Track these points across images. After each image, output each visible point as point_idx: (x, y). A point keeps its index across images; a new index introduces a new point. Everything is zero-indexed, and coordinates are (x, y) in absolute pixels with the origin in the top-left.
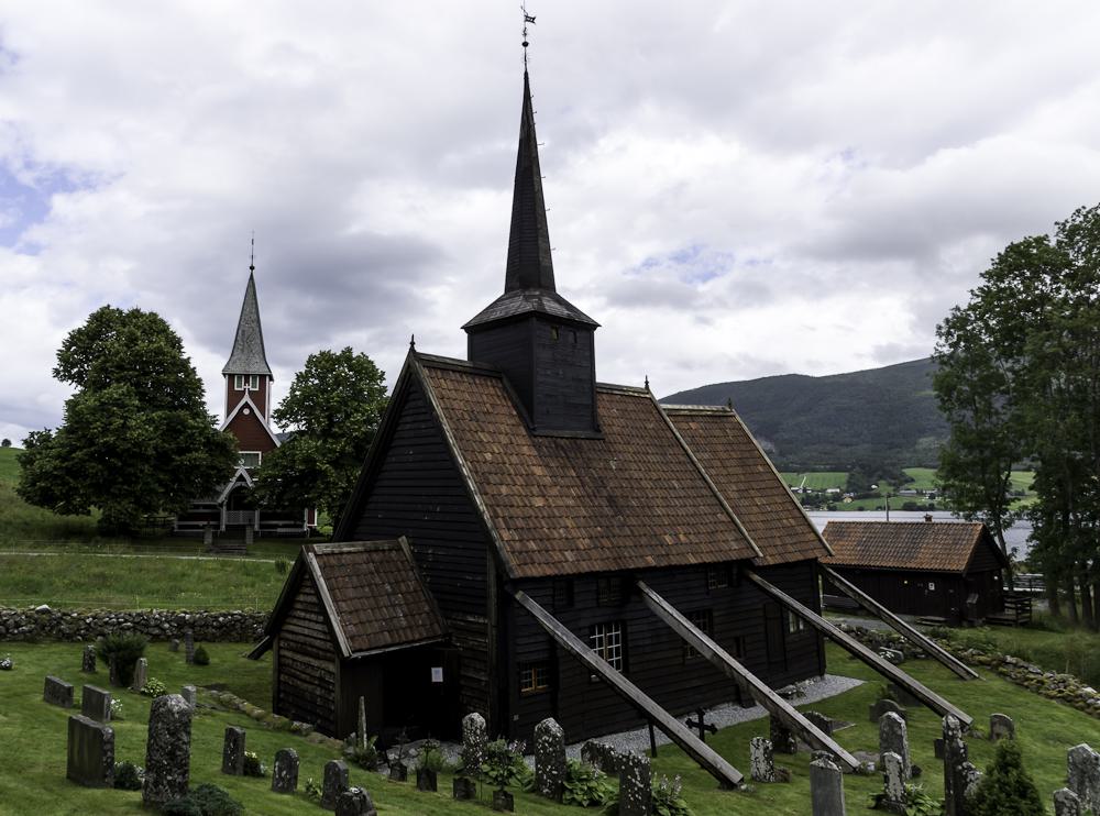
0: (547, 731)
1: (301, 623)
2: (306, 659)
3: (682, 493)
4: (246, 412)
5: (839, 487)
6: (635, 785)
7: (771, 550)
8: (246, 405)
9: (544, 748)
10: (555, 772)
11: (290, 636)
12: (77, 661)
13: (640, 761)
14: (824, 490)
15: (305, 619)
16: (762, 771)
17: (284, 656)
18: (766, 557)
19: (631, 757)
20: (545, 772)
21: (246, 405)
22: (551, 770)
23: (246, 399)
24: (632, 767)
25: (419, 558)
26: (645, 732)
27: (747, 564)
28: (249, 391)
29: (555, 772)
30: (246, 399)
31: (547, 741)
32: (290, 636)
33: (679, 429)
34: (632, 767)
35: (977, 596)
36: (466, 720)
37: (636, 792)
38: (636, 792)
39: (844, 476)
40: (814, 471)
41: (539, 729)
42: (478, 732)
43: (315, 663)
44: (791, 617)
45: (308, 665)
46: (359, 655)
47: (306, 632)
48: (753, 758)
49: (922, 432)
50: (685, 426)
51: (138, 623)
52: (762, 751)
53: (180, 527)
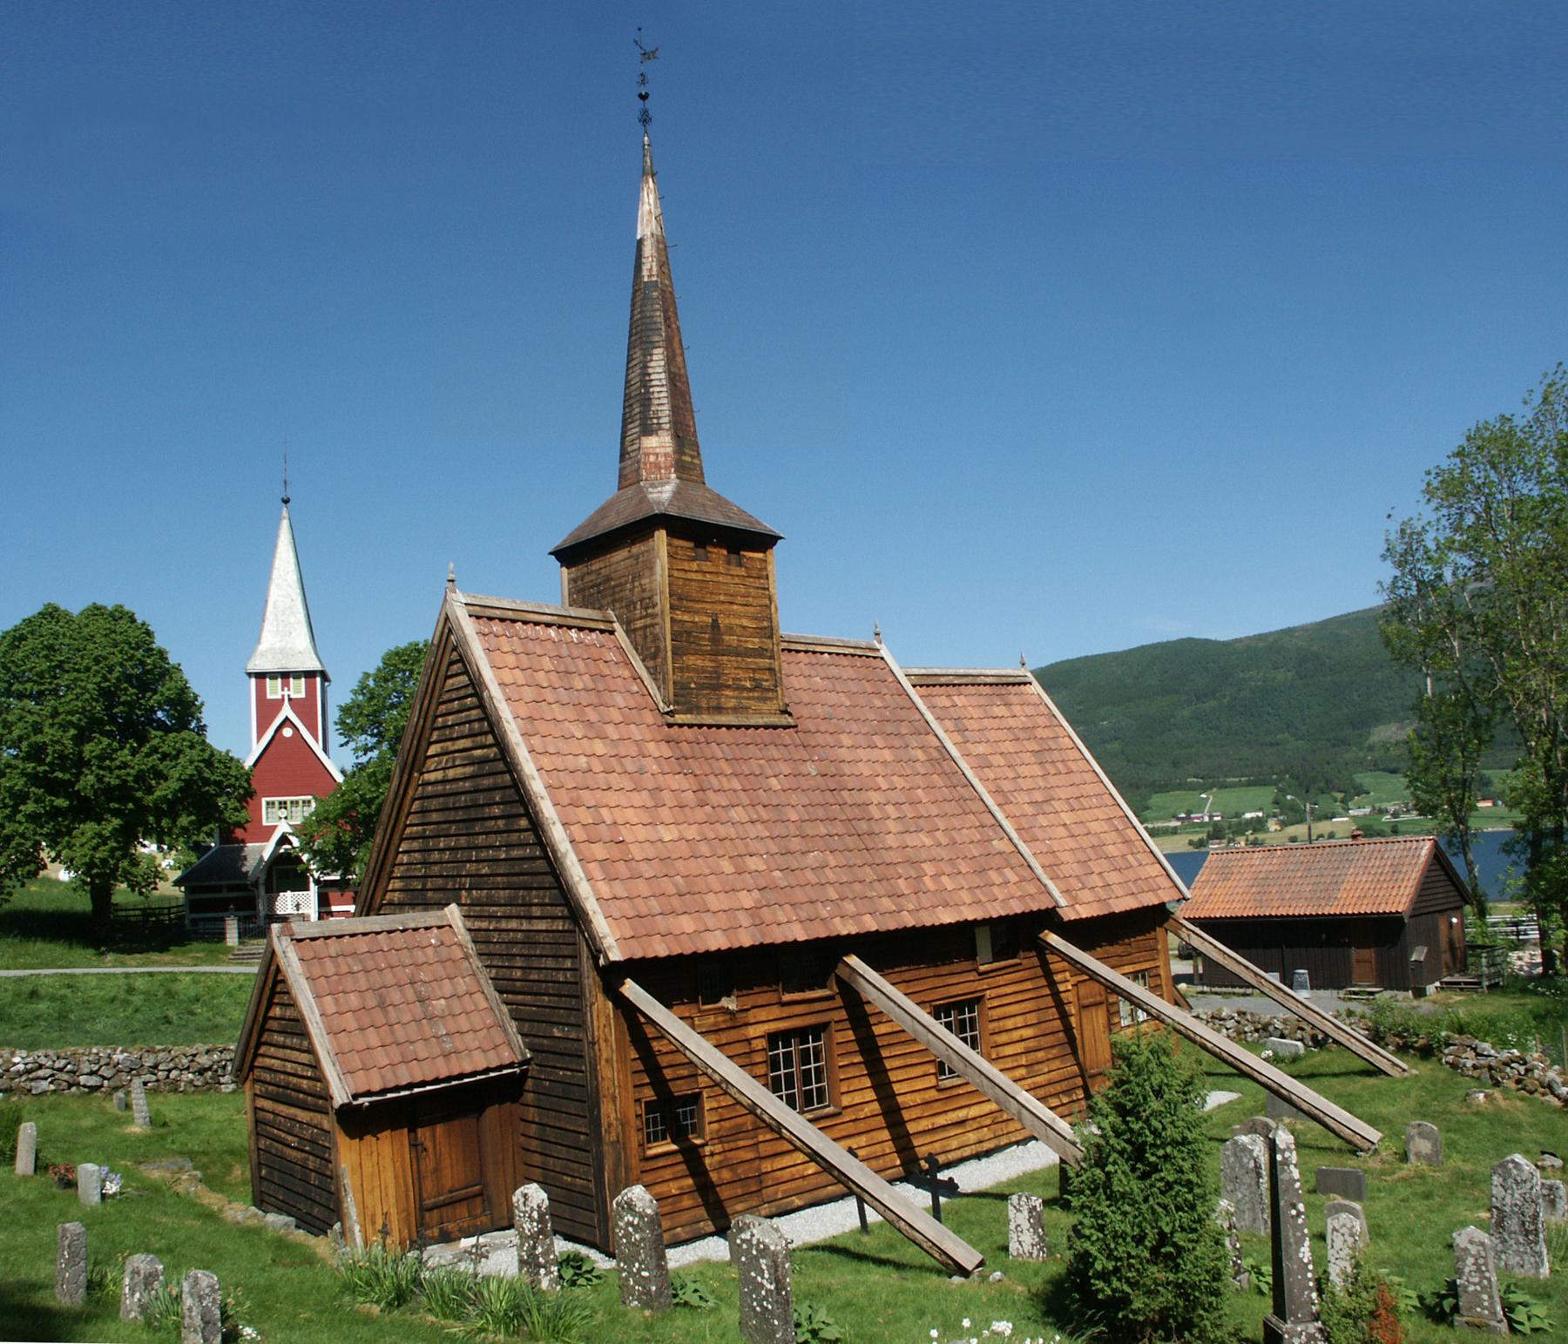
0: (630, 1207)
1: (281, 1053)
2: (292, 1111)
3: (934, 810)
4: (288, 732)
5: (1260, 809)
6: (763, 1286)
7: (1086, 895)
8: (287, 721)
9: (628, 1235)
10: (645, 1274)
11: (267, 1076)
12: (428, 1134)
13: (766, 1247)
14: (1238, 815)
15: (284, 1047)
16: (1027, 1247)
17: (262, 1109)
18: (1074, 910)
19: (754, 1242)
20: (630, 1273)
21: (287, 721)
22: (639, 1270)
23: (287, 711)
24: (756, 1258)
25: (478, 936)
26: (852, 1203)
27: (1049, 918)
28: (290, 699)
29: (645, 1274)
30: (287, 711)
31: (631, 1224)
32: (267, 1076)
33: (932, 707)
34: (756, 1258)
35: (1426, 950)
36: (517, 1197)
37: (765, 1298)
38: (765, 1298)
39: (1268, 794)
40: (1224, 786)
41: (618, 1204)
42: (535, 1215)
43: (303, 1115)
44: (1125, 1008)
45: (293, 1119)
46: (365, 1101)
47: (289, 1067)
48: (1012, 1226)
49: (1377, 718)
50: (943, 701)
51: (61, 1070)
52: (1026, 1213)
53: (194, 922)
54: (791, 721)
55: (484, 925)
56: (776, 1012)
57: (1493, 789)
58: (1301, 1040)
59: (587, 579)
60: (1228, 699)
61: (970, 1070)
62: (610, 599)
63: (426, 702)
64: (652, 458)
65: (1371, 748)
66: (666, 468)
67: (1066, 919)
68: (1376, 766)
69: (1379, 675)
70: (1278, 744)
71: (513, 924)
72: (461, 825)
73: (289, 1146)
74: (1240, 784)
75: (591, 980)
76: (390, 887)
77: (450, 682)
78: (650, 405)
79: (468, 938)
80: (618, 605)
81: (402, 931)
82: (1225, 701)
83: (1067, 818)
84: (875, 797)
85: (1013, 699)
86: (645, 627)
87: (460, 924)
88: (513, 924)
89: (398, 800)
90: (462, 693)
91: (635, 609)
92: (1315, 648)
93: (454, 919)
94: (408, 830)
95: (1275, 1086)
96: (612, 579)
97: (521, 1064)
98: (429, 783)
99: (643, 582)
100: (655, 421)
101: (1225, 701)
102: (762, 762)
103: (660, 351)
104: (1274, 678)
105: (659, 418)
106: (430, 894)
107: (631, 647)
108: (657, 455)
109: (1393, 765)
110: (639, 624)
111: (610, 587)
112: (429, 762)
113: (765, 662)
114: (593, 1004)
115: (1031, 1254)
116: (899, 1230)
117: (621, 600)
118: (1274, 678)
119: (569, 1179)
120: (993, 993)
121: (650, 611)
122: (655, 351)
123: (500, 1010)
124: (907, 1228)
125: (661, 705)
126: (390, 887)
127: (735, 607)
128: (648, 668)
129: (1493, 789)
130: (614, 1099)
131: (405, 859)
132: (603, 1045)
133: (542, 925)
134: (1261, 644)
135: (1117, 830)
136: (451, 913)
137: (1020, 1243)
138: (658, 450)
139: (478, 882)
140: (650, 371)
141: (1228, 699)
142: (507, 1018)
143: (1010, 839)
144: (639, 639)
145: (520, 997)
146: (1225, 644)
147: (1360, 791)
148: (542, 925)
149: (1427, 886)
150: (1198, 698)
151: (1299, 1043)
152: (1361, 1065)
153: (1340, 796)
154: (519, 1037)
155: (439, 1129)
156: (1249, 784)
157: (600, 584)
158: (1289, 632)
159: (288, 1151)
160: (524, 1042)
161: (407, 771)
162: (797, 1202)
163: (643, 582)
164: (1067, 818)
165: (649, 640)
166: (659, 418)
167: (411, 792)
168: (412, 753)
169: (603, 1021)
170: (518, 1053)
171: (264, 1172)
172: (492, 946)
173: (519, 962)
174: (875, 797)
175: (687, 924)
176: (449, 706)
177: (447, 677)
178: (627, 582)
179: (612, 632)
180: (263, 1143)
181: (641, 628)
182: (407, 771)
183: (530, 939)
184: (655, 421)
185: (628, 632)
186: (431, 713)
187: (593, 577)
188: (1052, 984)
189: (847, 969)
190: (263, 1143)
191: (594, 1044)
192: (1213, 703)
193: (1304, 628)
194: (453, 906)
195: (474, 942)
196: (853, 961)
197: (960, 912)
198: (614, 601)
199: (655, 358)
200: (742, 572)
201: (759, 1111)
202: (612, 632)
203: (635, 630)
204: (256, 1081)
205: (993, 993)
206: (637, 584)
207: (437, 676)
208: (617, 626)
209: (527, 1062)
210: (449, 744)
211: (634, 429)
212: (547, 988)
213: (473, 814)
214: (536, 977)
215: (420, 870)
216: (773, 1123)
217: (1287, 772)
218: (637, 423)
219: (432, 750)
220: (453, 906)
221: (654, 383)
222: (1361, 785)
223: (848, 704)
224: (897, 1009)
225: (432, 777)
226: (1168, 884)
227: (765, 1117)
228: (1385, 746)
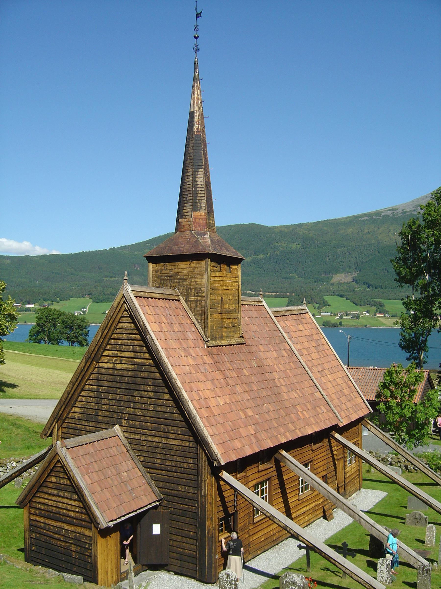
2: (60, 524)
27: (336, 428)
49: (336, 271)
54: (243, 341)
55: (137, 437)
56: (257, 475)
57: (384, 308)
58: (400, 467)
59: (164, 272)
60: (269, 254)
61: (338, 502)
62: (177, 284)
63: (106, 332)
64: (197, 220)
65: (332, 284)
66: (203, 226)
67: (340, 427)
68: (334, 293)
69: (339, 251)
70: (290, 279)
71: (156, 439)
72: (124, 390)
73: (60, 540)
74: (271, 296)
75: (206, 470)
76: (73, 411)
77: (121, 325)
78: (197, 196)
79: (126, 441)
80: (181, 288)
81: (102, 440)
82: (268, 255)
83: (330, 378)
84: (275, 374)
85: (304, 321)
86: (197, 301)
87: (122, 435)
88: (156, 439)
89: (83, 373)
90: (129, 331)
91: (191, 291)
92: (311, 235)
93: (119, 432)
94: (87, 387)
95: (426, 500)
96: (179, 275)
97: (158, 501)
98: (103, 368)
99: (197, 280)
100: (199, 205)
101: (268, 255)
102: (239, 362)
103: (202, 170)
104: (291, 247)
105: (200, 203)
106: (100, 418)
107: (188, 309)
108: (200, 219)
109: (342, 293)
110: (193, 299)
111: (177, 279)
112: (103, 358)
113: (235, 315)
114: (206, 480)
115: (386, 581)
116: (352, 577)
117: (183, 286)
118: (291, 247)
119: (181, 550)
120: (316, 458)
121: (200, 294)
122: (200, 170)
123: (147, 476)
124: (355, 576)
125: (204, 337)
126: (73, 411)
127: (228, 291)
128: (197, 320)
129: (384, 308)
130: (212, 520)
131: (84, 399)
132: (209, 497)
133: (174, 442)
134: (286, 230)
135: (346, 382)
136: (117, 430)
137: (382, 577)
138: (200, 217)
139: (133, 418)
140: (197, 179)
141: (269, 254)
142: (150, 480)
143: (320, 392)
144: (193, 305)
145: (158, 471)
146: (270, 228)
147: (326, 304)
148: (174, 442)
149: (425, 391)
150: (255, 253)
151: (399, 468)
152: (428, 481)
153: (317, 306)
154: (157, 488)
155: (105, 527)
156: (276, 296)
157: (171, 276)
158: (300, 226)
159: (59, 543)
160: (160, 491)
161: (90, 361)
162: (259, 552)
163: (197, 280)
164: (330, 378)
165: (198, 307)
166: (200, 203)
167: (91, 370)
168: (94, 353)
169: (210, 487)
170: (157, 495)
171: (33, 548)
172: (142, 447)
173: (159, 456)
174: (276, 375)
175: (237, 444)
176: (120, 336)
177: (119, 322)
178: (187, 279)
179: (179, 301)
180: (34, 535)
181: (194, 301)
182: (90, 361)
183: (166, 447)
184: (199, 205)
185: (186, 301)
186: (108, 337)
187: (168, 272)
188: (332, 452)
189: (281, 456)
190: (34, 535)
191: (205, 496)
192: (262, 256)
193: (307, 224)
194: (117, 426)
195: (130, 444)
196: (284, 453)
197: (313, 428)
198: (179, 286)
199: (199, 173)
200: (230, 275)
201: (288, 529)
202: (179, 301)
203: (191, 301)
204: (31, 507)
205: (316, 458)
206: (193, 280)
207: (114, 321)
208: (181, 297)
209: (161, 499)
210: (118, 353)
211: (188, 208)
212: (176, 469)
213: (133, 387)
214: (170, 464)
215: (95, 406)
216: (295, 534)
217: (294, 292)
218: (190, 204)
219: (106, 353)
220: (117, 426)
221: (199, 186)
222: (327, 302)
223: (258, 330)
224: (305, 475)
225: (105, 365)
226: (365, 406)
227: (292, 532)
228: (340, 284)
